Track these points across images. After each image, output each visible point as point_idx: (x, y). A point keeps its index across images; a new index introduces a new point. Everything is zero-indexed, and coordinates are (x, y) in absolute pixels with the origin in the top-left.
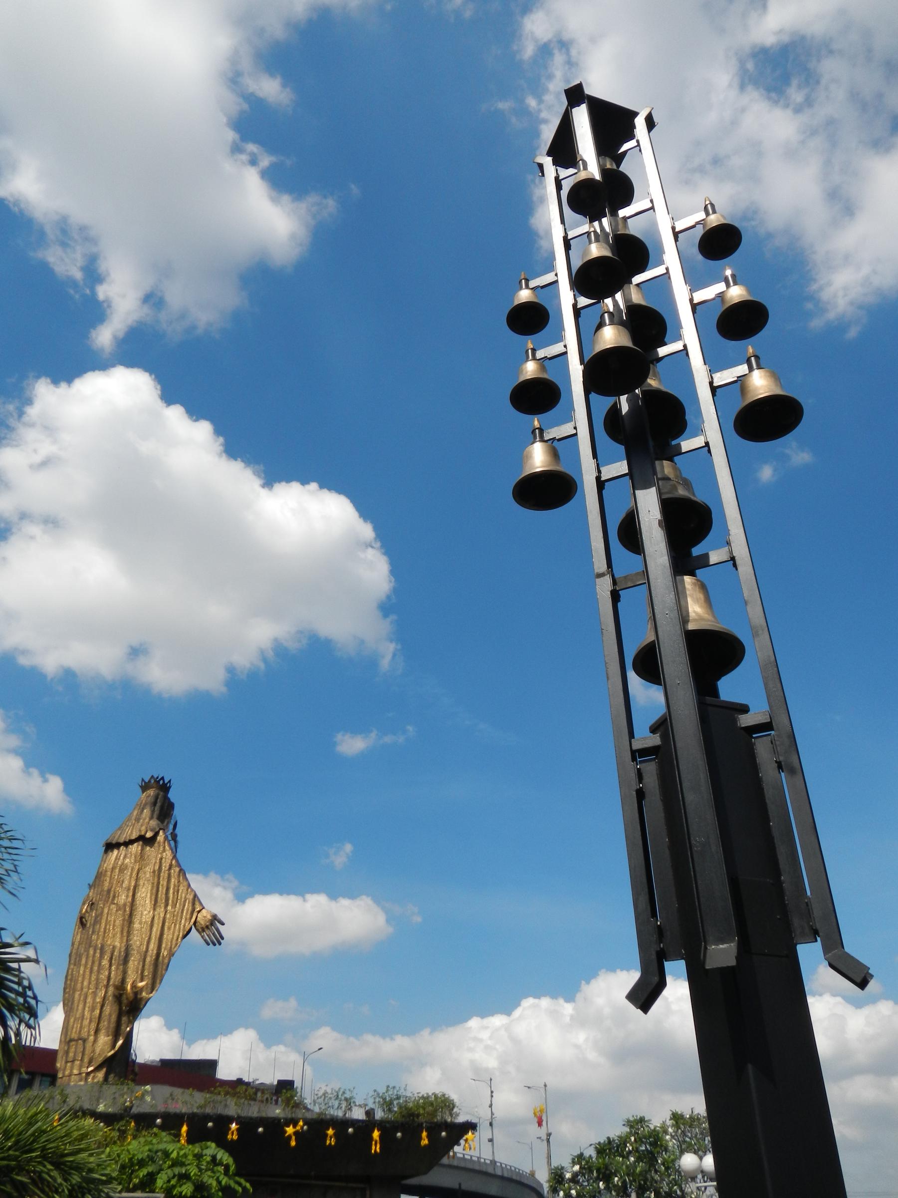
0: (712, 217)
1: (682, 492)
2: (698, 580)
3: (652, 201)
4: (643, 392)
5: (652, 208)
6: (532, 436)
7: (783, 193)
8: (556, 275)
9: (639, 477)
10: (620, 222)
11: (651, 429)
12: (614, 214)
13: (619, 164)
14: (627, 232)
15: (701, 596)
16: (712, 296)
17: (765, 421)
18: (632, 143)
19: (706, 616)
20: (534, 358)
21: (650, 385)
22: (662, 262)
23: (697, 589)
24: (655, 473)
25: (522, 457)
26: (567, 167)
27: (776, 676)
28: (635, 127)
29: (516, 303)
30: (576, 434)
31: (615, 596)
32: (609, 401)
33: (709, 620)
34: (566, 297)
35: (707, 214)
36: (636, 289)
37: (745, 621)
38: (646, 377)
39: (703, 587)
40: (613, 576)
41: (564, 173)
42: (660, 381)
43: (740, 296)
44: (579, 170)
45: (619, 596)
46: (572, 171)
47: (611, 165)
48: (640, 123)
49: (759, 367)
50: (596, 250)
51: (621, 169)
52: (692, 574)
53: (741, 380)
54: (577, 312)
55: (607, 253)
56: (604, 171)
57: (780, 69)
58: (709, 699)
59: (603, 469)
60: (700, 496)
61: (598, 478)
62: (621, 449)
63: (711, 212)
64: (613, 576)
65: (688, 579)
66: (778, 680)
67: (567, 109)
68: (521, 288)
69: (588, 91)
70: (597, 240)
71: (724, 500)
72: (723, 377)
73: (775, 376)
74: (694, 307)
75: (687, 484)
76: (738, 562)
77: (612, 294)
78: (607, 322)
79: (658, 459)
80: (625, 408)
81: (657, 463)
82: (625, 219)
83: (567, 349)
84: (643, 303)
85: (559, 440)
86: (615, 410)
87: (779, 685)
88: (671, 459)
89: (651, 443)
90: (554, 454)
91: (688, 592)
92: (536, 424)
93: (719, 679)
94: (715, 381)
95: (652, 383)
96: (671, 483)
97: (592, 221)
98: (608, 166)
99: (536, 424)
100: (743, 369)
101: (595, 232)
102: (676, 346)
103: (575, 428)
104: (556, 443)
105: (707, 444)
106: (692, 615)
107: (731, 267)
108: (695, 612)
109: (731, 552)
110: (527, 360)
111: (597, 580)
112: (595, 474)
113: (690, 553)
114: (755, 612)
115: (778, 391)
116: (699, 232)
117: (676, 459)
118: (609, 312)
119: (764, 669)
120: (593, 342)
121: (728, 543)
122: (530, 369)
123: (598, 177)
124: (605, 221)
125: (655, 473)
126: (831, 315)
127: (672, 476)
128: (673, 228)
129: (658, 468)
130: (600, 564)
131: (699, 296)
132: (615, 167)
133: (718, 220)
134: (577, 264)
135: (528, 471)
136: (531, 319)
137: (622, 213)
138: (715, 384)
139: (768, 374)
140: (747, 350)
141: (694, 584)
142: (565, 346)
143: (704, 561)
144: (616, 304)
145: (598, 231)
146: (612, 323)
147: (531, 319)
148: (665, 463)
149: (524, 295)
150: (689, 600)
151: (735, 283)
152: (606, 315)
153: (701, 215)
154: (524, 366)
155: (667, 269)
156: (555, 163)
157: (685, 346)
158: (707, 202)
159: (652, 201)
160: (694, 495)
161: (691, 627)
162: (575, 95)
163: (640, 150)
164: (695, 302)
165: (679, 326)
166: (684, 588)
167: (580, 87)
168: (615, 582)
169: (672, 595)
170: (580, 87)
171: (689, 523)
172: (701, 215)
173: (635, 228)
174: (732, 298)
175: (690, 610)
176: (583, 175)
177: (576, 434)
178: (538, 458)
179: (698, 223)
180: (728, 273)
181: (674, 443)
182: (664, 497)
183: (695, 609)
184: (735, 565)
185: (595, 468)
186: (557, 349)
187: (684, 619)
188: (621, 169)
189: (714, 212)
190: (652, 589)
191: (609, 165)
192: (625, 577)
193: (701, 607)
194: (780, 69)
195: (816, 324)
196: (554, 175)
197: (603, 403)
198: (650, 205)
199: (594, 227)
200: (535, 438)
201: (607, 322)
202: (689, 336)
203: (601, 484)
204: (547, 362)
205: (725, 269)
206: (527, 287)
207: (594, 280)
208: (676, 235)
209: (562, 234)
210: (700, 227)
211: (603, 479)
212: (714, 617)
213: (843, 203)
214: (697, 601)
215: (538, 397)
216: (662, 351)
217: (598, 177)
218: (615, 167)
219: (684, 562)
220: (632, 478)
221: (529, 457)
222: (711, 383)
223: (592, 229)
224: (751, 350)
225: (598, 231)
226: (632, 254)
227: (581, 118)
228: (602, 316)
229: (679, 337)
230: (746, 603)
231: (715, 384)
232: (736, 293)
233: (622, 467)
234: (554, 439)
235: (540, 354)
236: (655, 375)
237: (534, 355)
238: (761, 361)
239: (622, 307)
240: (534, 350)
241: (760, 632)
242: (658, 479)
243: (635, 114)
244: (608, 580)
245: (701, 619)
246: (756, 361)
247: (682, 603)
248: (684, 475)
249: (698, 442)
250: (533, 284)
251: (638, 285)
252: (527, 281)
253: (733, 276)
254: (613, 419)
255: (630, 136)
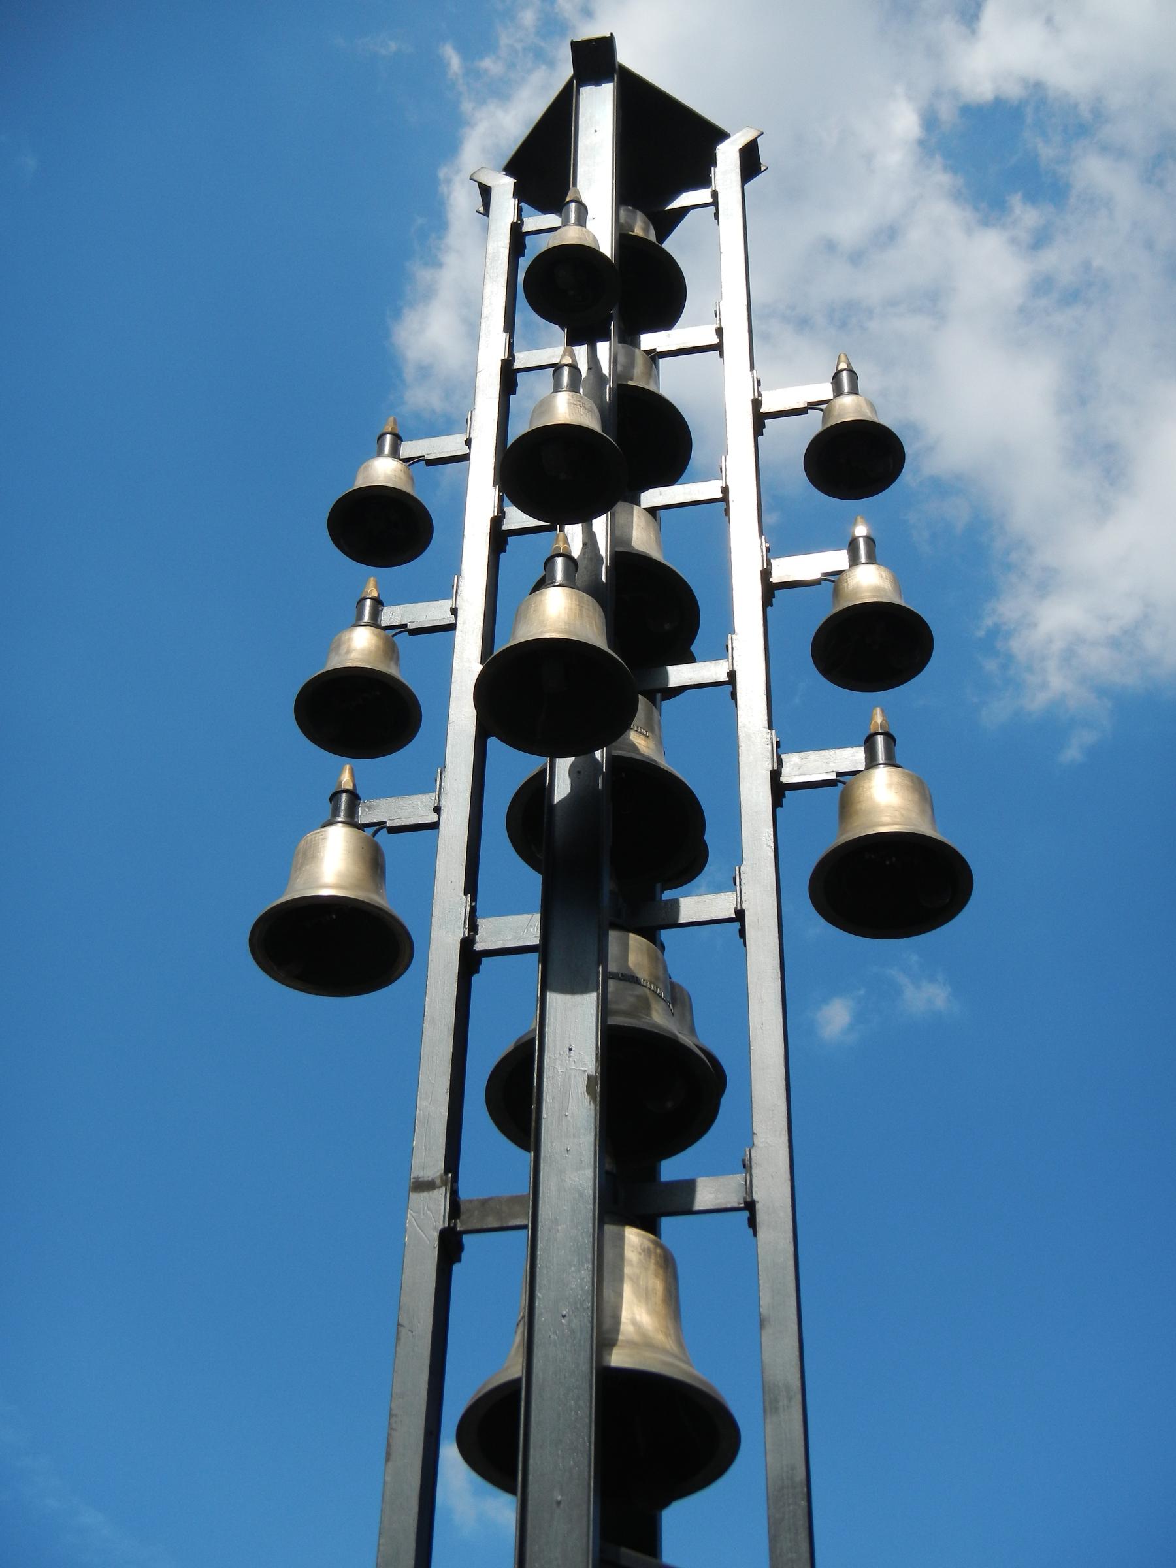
0: (847, 401)
1: (659, 1018)
2: (658, 1244)
3: (720, 332)
4: (612, 760)
5: (718, 347)
6: (329, 807)
7: (977, 403)
8: (468, 442)
9: (561, 960)
10: (640, 361)
11: (617, 853)
12: (629, 337)
13: (663, 234)
14: (651, 387)
15: (657, 1285)
16: (815, 575)
17: (884, 888)
18: (700, 196)
19: (660, 1338)
20: (374, 622)
21: (634, 747)
22: (715, 472)
23: (652, 1266)
24: (602, 958)
25: (293, 852)
26: (545, 209)
27: (802, 1522)
28: (715, 165)
29: (360, 483)
30: (435, 826)
31: (450, 1247)
32: (528, 764)
33: (665, 1351)
34: (481, 496)
35: (838, 391)
36: (639, 525)
37: (748, 1375)
38: (625, 724)
39: (667, 1264)
40: (454, 1194)
41: (535, 221)
42: (660, 743)
43: (877, 589)
44: (566, 222)
45: (460, 1247)
46: (552, 220)
47: (646, 230)
48: (727, 156)
49: (891, 762)
50: (565, 409)
51: (668, 245)
52: (650, 1225)
53: (844, 780)
54: (499, 538)
55: (590, 420)
56: (623, 239)
57: (1001, 154)
58: (628, 1554)
59: (483, 923)
60: (705, 1035)
61: (467, 944)
62: (533, 881)
63: (846, 388)
64: (454, 1194)
65: (633, 1237)
66: (803, 1534)
67: (569, 86)
68: (380, 453)
69: (625, 57)
70: (574, 387)
71: (755, 1057)
72: (802, 767)
73: (923, 791)
74: (770, 590)
75: (676, 998)
76: (761, 1216)
77: (585, 518)
78: (559, 576)
79: (615, 926)
80: (562, 788)
81: (613, 935)
82: (654, 356)
83: (458, 614)
84: (656, 554)
85: (394, 830)
86: (538, 787)
87: (805, 1547)
88: (650, 934)
89: (608, 885)
90: (374, 863)
91: (627, 1270)
92: (346, 779)
93: (666, 1503)
94: (785, 771)
95: (640, 742)
96: (639, 991)
97: (573, 340)
98: (638, 231)
99: (346, 779)
100: (852, 757)
101: (574, 367)
102: (715, 671)
103: (437, 810)
104: (382, 837)
105: (740, 915)
106: (627, 1328)
107: (868, 522)
108: (634, 1323)
109: (749, 1189)
110: (357, 622)
111: (415, 1197)
112: (461, 932)
113: (654, 1172)
114: (779, 1350)
115: (925, 828)
116: (813, 424)
117: (665, 935)
118: (568, 557)
119: (775, 1500)
120: (517, 615)
121: (747, 1166)
122: (360, 646)
123: (606, 248)
124: (604, 349)
125: (602, 957)
126: (1036, 703)
127: (643, 975)
128: (757, 403)
129: (613, 949)
130: (429, 1158)
131: (786, 569)
132: (652, 237)
133: (858, 408)
134: (517, 430)
135: (300, 889)
136: (387, 529)
137: (650, 341)
138: (785, 779)
139: (907, 782)
140: (871, 717)
141: (647, 1252)
142: (454, 611)
143: (680, 1199)
144: (590, 540)
145: (583, 367)
146: (569, 583)
147: (387, 529)
148: (634, 939)
149: (383, 471)
150: (628, 1290)
151: (872, 559)
152: (559, 561)
153: (825, 391)
154: (345, 636)
155: (725, 490)
156: (520, 193)
157: (732, 675)
158: (843, 366)
159: (720, 332)
160: (692, 1030)
161: (618, 1359)
162: (594, 60)
163: (716, 216)
164: (775, 578)
165: (727, 625)
166: (621, 1256)
167: (606, 45)
168: (455, 1209)
169: (586, 1273)
170: (606, 45)
171: (662, 1095)
172: (825, 391)
173: (673, 383)
174: (856, 591)
175: (625, 1315)
176: (571, 235)
177: (435, 826)
178: (331, 864)
179: (813, 405)
180: (861, 531)
181: (667, 895)
182: (615, 1021)
183: (638, 1314)
184: (752, 1223)
185: (466, 910)
186: (433, 613)
187: (604, 1334)
188: (668, 245)
189: (854, 390)
190: (540, 1245)
191: (640, 228)
192: (484, 1203)
193: (652, 1312)
194: (1001, 154)
195: (996, 713)
196: (510, 217)
197: (513, 766)
198: (715, 340)
199: (572, 355)
200: (335, 812)
201: (559, 576)
202: (743, 653)
203: (470, 959)
204: (403, 639)
205: (854, 523)
206: (395, 453)
207: (549, 474)
208: (760, 419)
209: (502, 354)
210: (815, 416)
211: (479, 946)
212: (680, 1343)
213: (1102, 461)
214: (645, 1295)
215: (363, 715)
216: (678, 675)
217: (606, 248)
218: (652, 237)
219: (633, 1190)
220: (544, 961)
221: (311, 855)
222: (775, 775)
223: (568, 360)
224: (878, 719)
225: (583, 367)
226: (647, 439)
227: (598, 111)
228: (549, 563)
229: (723, 651)
230: (762, 1323)
231: (785, 779)
232: (869, 582)
233: (522, 928)
234: (380, 825)
235: (391, 615)
236: (650, 728)
237: (375, 614)
238: (898, 749)
239: (603, 552)
240: (378, 603)
241: (783, 1402)
242: (608, 976)
243: (722, 136)
244: (439, 1200)
245: (646, 1343)
246: (885, 747)
247: (607, 1293)
248: (675, 979)
249: (721, 905)
250: (409, 449)
251: (653, 511)
252: (398, 439)
253: (869, 540)
254: (530, 813)
255: (701, 177)
